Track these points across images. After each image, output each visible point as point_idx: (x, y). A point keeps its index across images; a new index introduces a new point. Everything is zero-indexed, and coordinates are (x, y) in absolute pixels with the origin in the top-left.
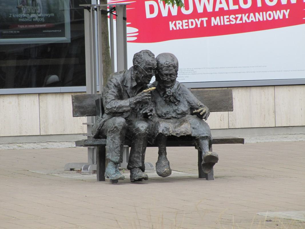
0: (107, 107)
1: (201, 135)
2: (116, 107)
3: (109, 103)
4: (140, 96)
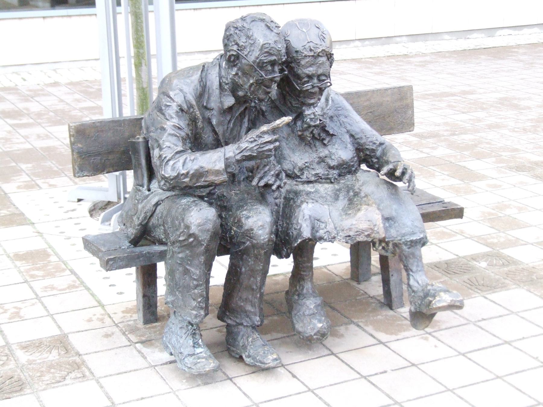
0: (163, 173)
1: (407, 235)
2: (188, 173)
3: (169, 160)
4: (252, 142)
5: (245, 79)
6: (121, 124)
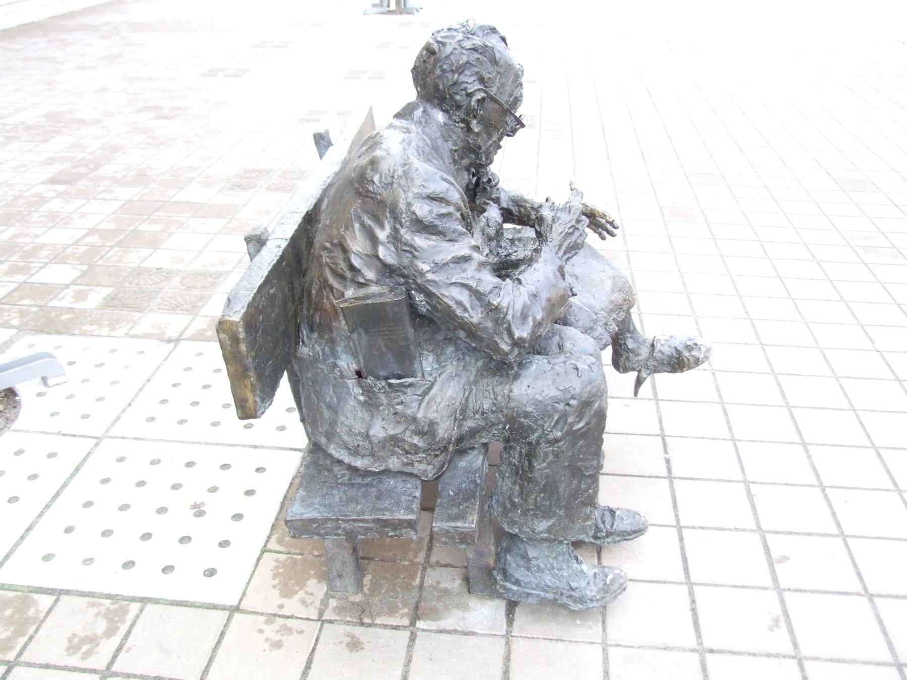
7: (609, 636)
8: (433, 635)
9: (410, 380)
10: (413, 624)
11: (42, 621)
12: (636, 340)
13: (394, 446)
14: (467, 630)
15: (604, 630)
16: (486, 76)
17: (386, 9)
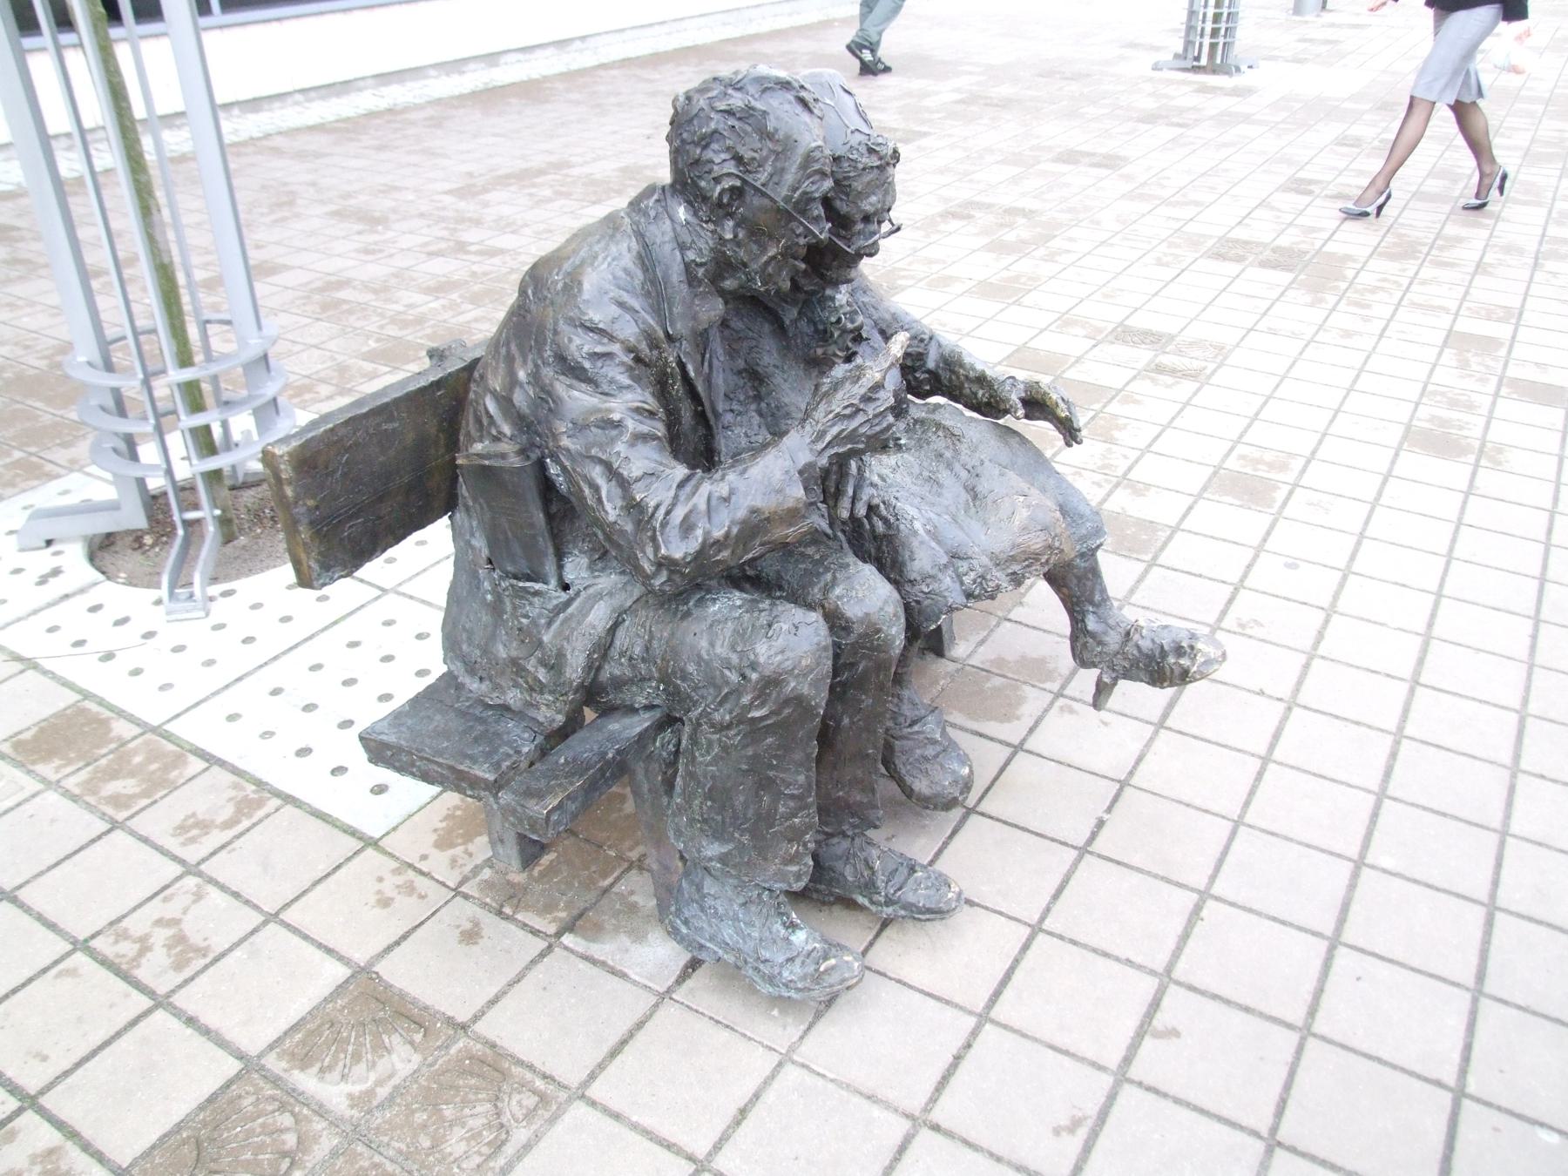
5: (755, 247)
6: (392, 414)
7: (803, 1048)
8: (573, 957)
9: (538, 586)
10: (559, 934)
11: (176, 788)
12: (1101, 619)
13: (517, 673)
14: (619, 968)
15: (802, 1038)
16: (748, 155)
17: (1189, 63)
